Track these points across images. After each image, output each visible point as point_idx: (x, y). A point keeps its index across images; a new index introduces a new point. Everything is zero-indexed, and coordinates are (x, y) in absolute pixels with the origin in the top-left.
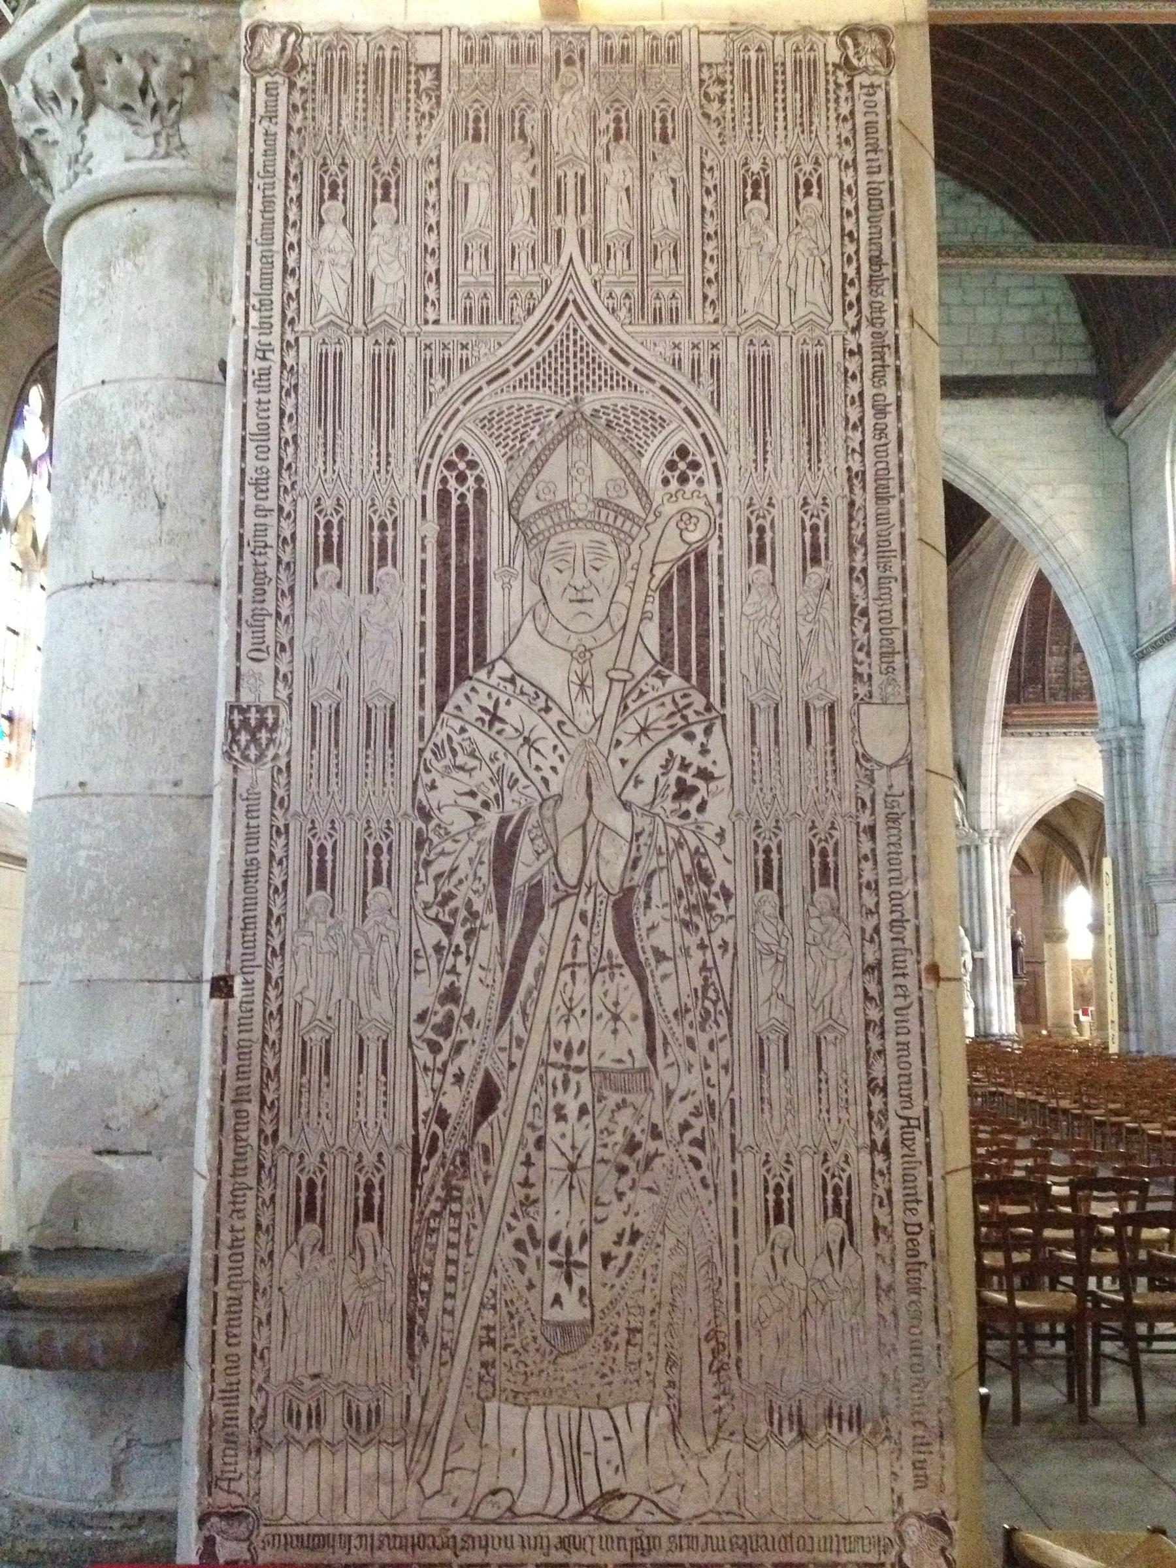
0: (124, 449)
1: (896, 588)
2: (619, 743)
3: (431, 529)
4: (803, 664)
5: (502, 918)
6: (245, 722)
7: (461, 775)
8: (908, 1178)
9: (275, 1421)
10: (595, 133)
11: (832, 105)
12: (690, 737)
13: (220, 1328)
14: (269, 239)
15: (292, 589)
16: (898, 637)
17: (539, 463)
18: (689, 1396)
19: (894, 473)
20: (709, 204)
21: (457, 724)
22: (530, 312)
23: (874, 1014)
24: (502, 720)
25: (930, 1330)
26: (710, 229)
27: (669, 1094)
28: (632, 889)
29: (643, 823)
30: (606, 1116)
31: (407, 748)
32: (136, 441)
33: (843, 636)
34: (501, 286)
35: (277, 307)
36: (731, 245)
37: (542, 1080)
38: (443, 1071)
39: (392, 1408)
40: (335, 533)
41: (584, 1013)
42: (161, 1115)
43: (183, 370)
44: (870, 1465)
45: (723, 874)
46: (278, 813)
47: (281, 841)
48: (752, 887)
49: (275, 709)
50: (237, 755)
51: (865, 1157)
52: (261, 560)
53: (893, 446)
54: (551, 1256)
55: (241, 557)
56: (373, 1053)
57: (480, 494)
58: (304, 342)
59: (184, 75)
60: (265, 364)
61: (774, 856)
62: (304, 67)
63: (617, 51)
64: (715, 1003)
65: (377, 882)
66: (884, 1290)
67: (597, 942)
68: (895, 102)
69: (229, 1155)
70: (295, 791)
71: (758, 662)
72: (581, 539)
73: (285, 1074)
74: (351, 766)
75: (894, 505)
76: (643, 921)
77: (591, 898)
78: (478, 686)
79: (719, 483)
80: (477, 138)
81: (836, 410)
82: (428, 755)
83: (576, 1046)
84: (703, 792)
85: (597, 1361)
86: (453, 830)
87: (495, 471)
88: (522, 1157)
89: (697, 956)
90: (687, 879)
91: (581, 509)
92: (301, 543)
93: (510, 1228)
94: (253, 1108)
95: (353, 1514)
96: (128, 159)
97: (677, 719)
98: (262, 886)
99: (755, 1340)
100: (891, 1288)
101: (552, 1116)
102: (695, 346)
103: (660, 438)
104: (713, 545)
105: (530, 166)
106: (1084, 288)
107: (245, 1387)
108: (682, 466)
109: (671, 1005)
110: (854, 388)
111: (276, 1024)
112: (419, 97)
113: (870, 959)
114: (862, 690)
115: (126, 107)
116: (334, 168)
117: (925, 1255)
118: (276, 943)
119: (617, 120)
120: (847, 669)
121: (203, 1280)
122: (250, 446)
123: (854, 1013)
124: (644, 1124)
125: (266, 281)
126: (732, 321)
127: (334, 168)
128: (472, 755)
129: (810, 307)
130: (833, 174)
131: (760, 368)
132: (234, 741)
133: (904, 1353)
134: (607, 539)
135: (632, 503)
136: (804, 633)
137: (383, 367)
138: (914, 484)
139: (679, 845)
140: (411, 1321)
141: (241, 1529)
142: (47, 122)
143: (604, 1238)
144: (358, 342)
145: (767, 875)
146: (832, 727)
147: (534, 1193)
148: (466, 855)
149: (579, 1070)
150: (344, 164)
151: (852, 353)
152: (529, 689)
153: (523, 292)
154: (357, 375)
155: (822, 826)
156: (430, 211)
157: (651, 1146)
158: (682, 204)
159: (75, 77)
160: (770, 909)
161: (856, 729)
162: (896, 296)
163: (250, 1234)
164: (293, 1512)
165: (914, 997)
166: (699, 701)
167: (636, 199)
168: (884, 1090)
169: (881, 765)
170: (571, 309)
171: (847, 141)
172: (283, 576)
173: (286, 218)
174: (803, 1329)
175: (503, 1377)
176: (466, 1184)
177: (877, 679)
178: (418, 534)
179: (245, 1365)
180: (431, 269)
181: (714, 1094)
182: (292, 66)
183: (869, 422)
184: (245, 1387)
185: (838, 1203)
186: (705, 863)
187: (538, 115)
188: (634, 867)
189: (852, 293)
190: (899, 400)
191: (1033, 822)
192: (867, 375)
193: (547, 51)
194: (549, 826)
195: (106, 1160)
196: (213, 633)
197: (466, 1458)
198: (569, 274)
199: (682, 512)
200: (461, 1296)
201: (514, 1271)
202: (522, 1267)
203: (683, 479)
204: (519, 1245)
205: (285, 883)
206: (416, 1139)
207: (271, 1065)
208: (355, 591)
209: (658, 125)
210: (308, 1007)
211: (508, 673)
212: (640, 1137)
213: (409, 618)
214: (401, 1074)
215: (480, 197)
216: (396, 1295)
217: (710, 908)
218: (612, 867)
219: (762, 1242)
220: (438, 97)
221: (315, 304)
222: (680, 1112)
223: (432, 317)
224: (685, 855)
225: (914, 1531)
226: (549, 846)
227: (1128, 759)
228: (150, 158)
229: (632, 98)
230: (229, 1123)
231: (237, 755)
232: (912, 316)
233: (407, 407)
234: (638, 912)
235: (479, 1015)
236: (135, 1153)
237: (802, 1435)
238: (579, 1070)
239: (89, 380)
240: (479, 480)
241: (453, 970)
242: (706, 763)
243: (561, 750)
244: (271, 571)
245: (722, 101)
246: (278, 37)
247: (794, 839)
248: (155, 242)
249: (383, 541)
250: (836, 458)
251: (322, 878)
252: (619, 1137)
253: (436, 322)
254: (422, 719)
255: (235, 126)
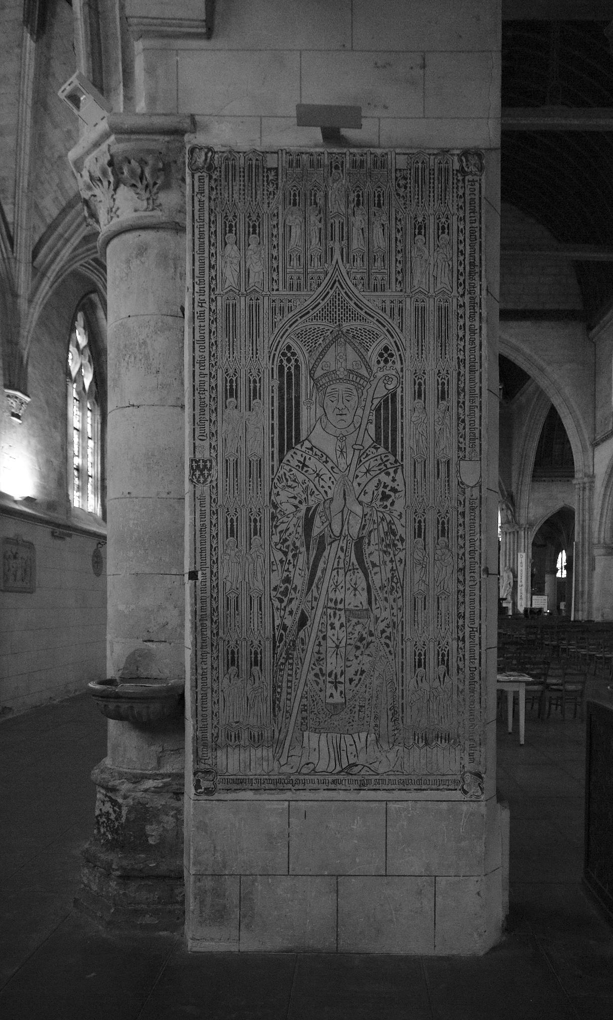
0: (140, 346)
1: (477, 410)
2: (357, 476)
3: (276, 383)
4: (437, 444)
5: (308, 549)
6: (198, 467)
7: (290, 490)
8: (472, 651)
9: (222, 740)
10: (348, 203)
11: (455, 190)
12: (388, 474)
13: (199, 704)
14: (202, 251)
15: (216, 409)
16: (477, 432)
17: (323, 354)
18: (383, 731)
19: (477, 360)
20: (399, 237)
21: (288, 468)
22: (319, 285)
23: (461, 588)
24: (307, 467)
25: (477, 706)
26: (399, 249)
27: (377, 619)
28: (363, 538)
29: (367, 510)
30: (351, 627)
31: (267, 478)
32: (145, 343)
33: (454, 432)
34: (306, 273)
35: (207, 282)
36: (408, 255)
37: (325, 613)
38: (285, 610)
39: (267, 734)
40: (234, 384)
41: (342, 587)
42: (169, 627)
43: (164, 311)
44: (452, 755)
45: (401, 531)
46: (213, 505)
47: (215, 517)
48: (413, 537)
49: (211, 461)
50: (195, 480)
51: (455, 643)
52: (202, 396)
53: (477, 348)
54: (329, 679)
55: (194, 395)
56: (256, 602)
57: (297, 367)
58: (219, 298)
59: (160, 170)
60: (202, 309)
61: (423, 524)
62: (216, 168)
63: (358, 163)
64: (396, 584)
65: (255, 534)
66: (460, 692)
67: (347, 559)
68: (483, 190)
69: (199, 640)
70: (220, 496)
71: (418, 441)
72: (341, 387)
73: (221, 610)
74: (243, 487)
75: (477, 374)
76: (367, 550)
77: (345, 541)
78: (297, 452)
79: (402, 363)
80: (295, 204)
81: (453, 331)
82: (276, 481)
83: (339, 601)
84: (393, 497)
85: (348, 716)
86: (287, 512)
87: (303, 356)
88: (317, 642)
89: (389, 565)
90: (386, 534)
91: (341, 374)
92: (220, 389)
93: (313, 669)
94: (208, 623)
95: (253, 772)
96: (136, 211)
97: (382, 466)
98: (208, 535)
99: (409, 710)
100: (463, 691)
101: (329, 627)
102: (392, 302)
103: (375, 344)
104: (399, 390)
105: (318, 217)
106: (581, 268)
107: (210, 726)
108: (386, 355)
109: (378, 584)
110: (461, 323)
111: (216, 591)
112: (268, 184)
113: (461, 566)
114: (461, 455)
115: (134, 186)
116: (230, 218)
117: (477, 678)
118: (214, 558)
119: (358, 196)
120: (455, 446)
121: (192, 687)
122: (197, 346)
123: (453, 587)
124: (366, 630)
125: (202, 271)
126: (408, 290)
127: (230, 218)
128: (294, 481)
129: (443, 285)
130: (455, 224)
131: (420, 312)
132: (193, 474)
133: (467, 715)
134: (353, 387)
135: (364, 372)
136: (437, 429)
137: (254, 310)
138: (486, 365)
139: (383, 519)
140: (274, 703)
141: (211, 777)
142: (97, 191)
143: (350, 673)
144: (243, 299)
145: (419, 532)
146: (448, 470)
147: (322, 656)
148: (293, 524)
149: (340, 610)
150: (235, 216)
151: (461, 306)
152: (319, 453)
153: (316, 276)
154: (243, 313)
155: (443, 511)
156: (274, 239)
157: (370, 639)
158: (386, 236)
159: (110, 170)
160: (420, 546)
161: (458, 471)
162: (480, 280)
163: (209, 671)
164: (229, 770)
165: (478, 581)
166: (392, 458)
167: (366, 234)
168: (464, 617)
169: (468, 486)
170: (337, 284)
171: (461, 208)
172: (212, 403)
173: (210, 241)
174: (428, 706)
175: (311, 723)
176: (295, 653)
177: (468, 450)
178: (270, 385)
179: (209, 719)
180: (275, 266)
181: (395, 620)
182: (210, 168)
183: (467, 337)
184: (210, 726)
185: (443, 660)
186: (393, 527)
187: (322, 193)
188: (363, 529)
189: (462, 279)
190: (480, 327)
191: (543, 521)
192: (467, 315)
193: (326, 162)
194: (328, 512)
195: (148, 644)
196: (182, 428)
197: (297, 751)
198: (336, 268)
199: (385, 376)
200: (293, 694)
201: (315, 685)
202: (318, 684)
203: (386, 361)
204: (316, 675)
205: (217, 534)
206: (274, 635)
207: (215, 606)
208: (243, 410)
209: (376, 199)
210: (229, 584)
211: (309, 446)
212: (365, 635)
213: (267, 424)
214: (267, 611)
215: (296, 232)
216: (268, 693)
217: (395, 545)
218: (355, 531)
219: (413, 674)
220: (277, 184)
221: (224, 282)
222: (382, 626)
223: (275, 287)
224: (385, 524)
225: (468, 778)
226: (328, 519)
227: (587, 492)
228: (145, 210)
229: (365, 185)
230: (199, 629)
231: (195, 480)
232: (487, 290)
233: (265, 328)
234: (365, 546)
235: (299, 588)
236: (161, 641)
237: (426, 744)
238: (340, 610)
239: (123, 315)
240: (296, 361)
241: (288, 570)
242: (394, 485)
243: (333, 479)
244: (207, 401)
245: (406, 188)
246: (203, 154)
247: (431, 517)
248: (149, 251)
249: (255, 387)
250: (453, 353)
251: (232, 532)
252: (356, 635)
253: (277, 290)
254: (273, 466)
255: (183, 195)
